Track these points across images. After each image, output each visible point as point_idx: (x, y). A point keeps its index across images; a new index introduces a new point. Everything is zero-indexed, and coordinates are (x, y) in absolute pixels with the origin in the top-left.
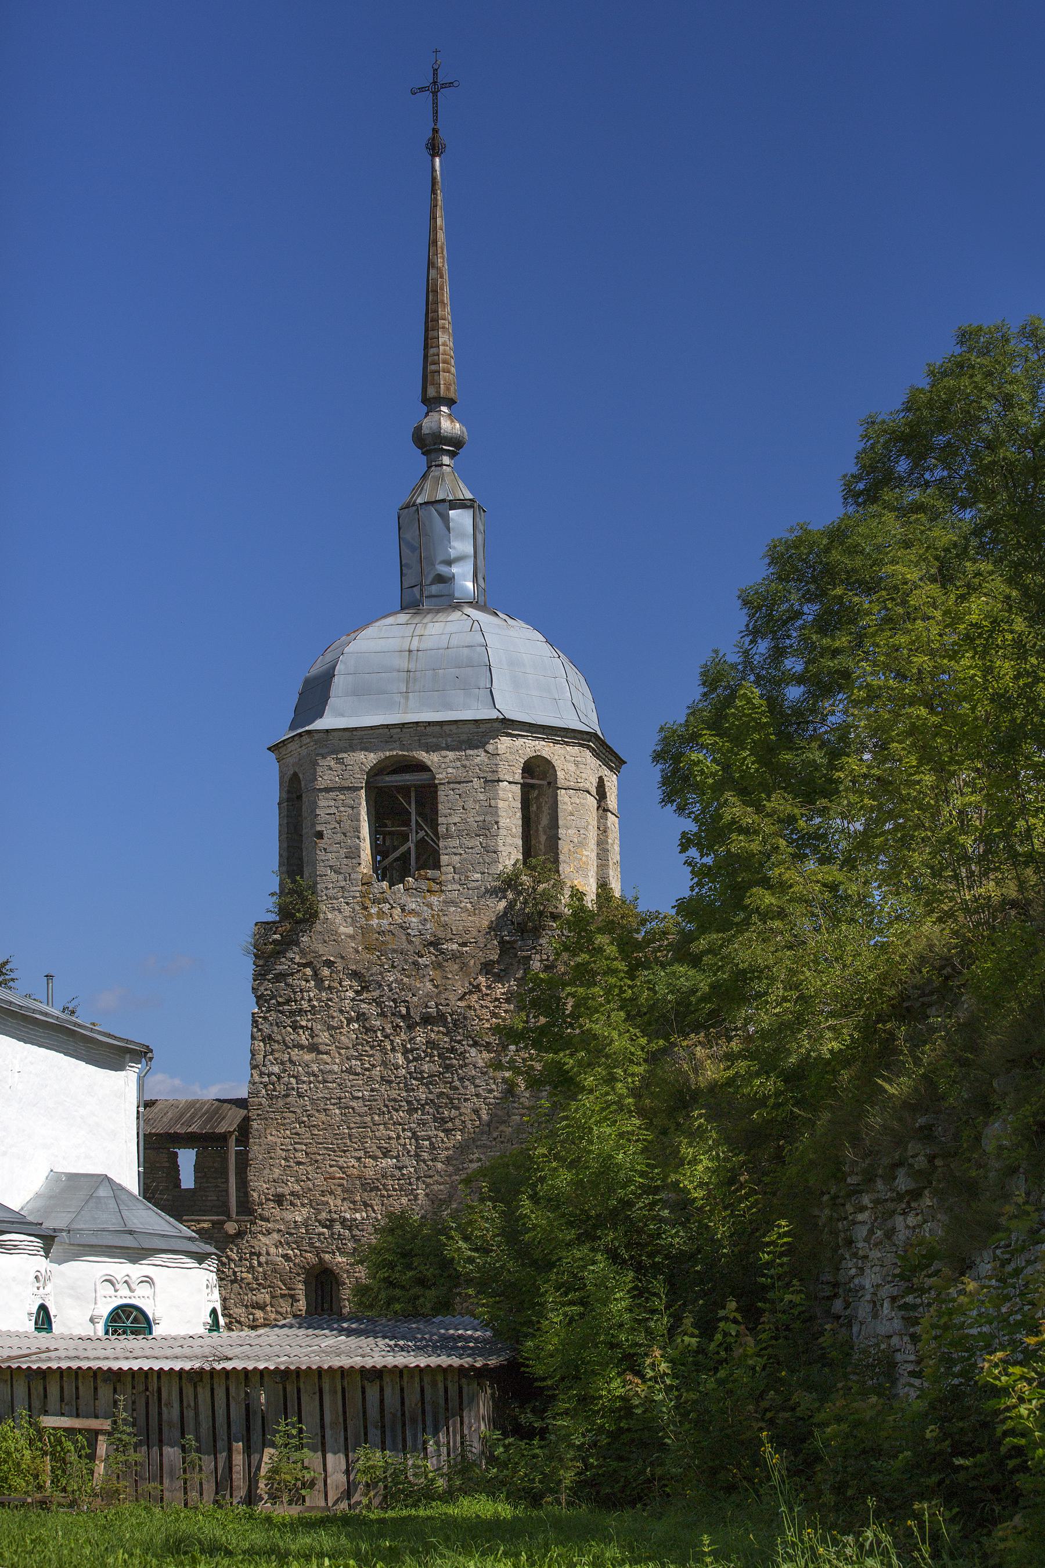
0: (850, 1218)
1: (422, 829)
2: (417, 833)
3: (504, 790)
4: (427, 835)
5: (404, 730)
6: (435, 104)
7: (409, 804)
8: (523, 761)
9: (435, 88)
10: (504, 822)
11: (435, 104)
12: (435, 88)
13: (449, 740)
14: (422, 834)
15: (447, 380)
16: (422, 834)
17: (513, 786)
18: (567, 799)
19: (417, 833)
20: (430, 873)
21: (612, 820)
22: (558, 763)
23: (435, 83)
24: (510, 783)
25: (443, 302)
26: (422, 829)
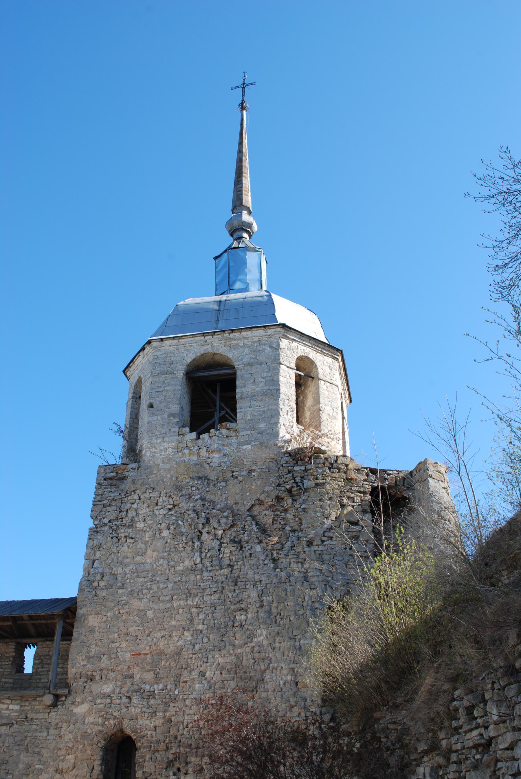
0: (311, 749)
1: (223, 409)
2: (220, 412)
3: (284, 370)
4: (227, 413)
5: (215, 337)
6: (243, 92)
7: (216, 394)
8: (296, 357)
9: (244, 86)
10: (283, 389)
11: (243, 92)
12: (244, 86)
13: (246, 341)
14: (223, 413)
15: (248, 200)
16: (223, 413)
17: (290, 370)
18: (325, 387)
19: (220, 412)
20: (229, 424)
21: (346, 422)
22: (319, 364)
23: (243, 84)
24: (288, 367)
25: (245, 167)
26: (223, 409)
